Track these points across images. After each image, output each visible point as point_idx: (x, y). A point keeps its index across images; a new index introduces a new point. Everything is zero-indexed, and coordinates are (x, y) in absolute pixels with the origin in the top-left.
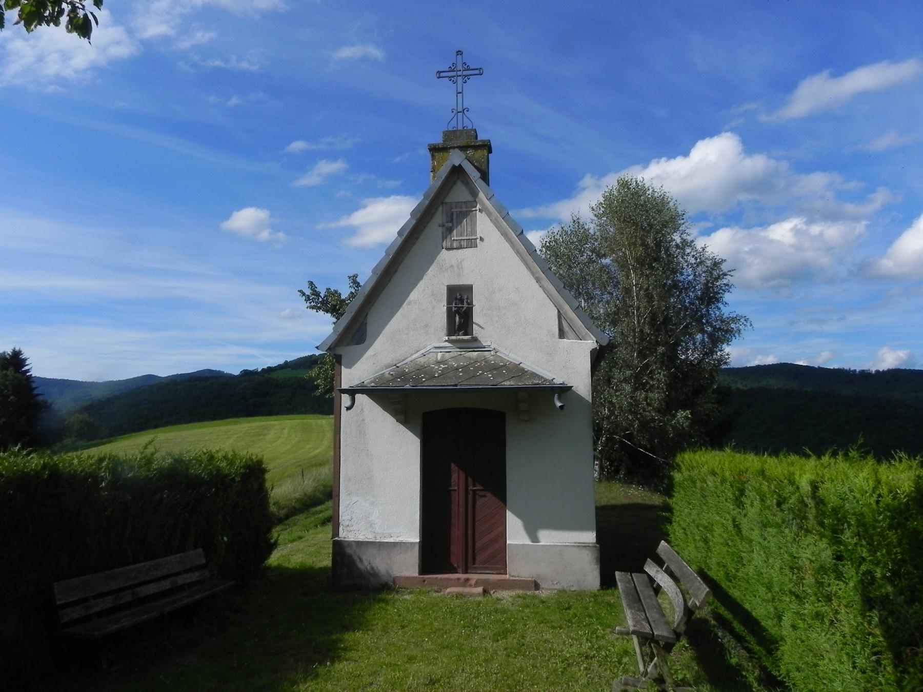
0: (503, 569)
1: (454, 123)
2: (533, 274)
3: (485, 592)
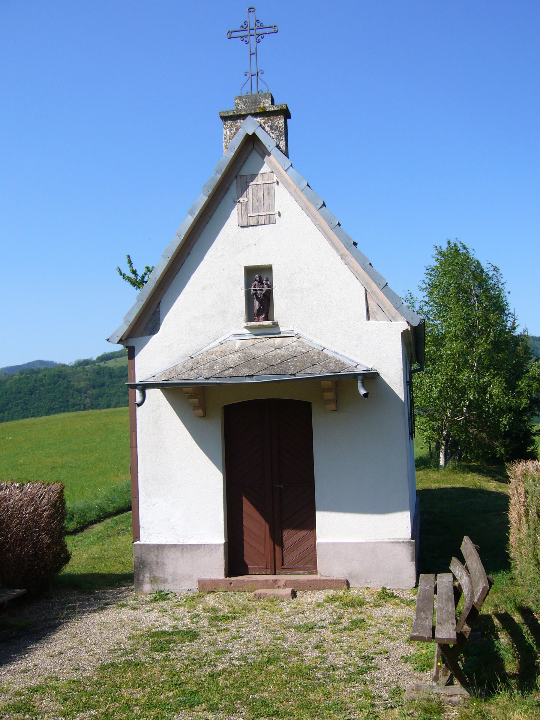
0: (313, 569)
1: (247, 88)
2: (336, 249)
3: (294, 594)
